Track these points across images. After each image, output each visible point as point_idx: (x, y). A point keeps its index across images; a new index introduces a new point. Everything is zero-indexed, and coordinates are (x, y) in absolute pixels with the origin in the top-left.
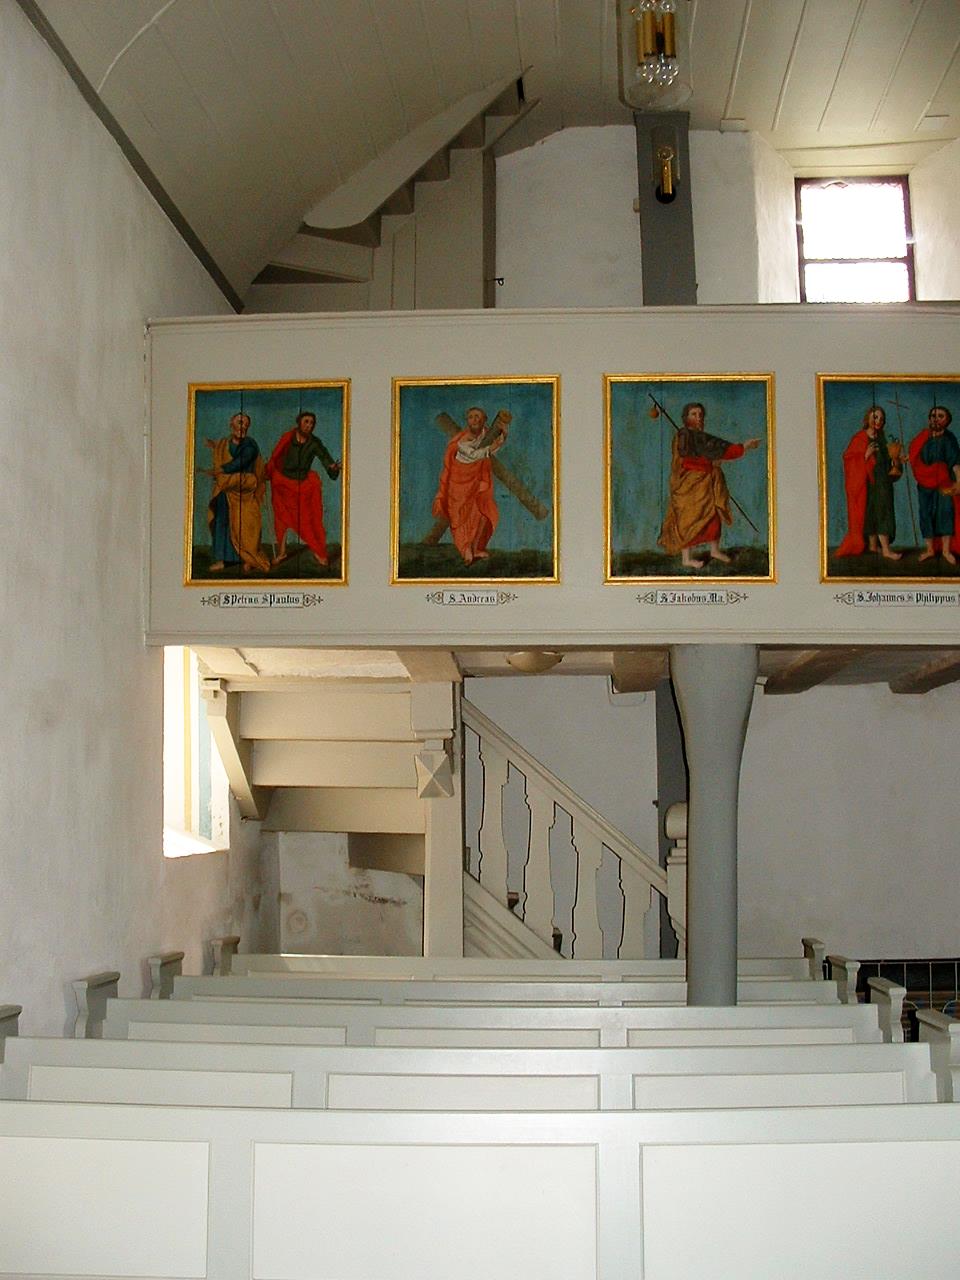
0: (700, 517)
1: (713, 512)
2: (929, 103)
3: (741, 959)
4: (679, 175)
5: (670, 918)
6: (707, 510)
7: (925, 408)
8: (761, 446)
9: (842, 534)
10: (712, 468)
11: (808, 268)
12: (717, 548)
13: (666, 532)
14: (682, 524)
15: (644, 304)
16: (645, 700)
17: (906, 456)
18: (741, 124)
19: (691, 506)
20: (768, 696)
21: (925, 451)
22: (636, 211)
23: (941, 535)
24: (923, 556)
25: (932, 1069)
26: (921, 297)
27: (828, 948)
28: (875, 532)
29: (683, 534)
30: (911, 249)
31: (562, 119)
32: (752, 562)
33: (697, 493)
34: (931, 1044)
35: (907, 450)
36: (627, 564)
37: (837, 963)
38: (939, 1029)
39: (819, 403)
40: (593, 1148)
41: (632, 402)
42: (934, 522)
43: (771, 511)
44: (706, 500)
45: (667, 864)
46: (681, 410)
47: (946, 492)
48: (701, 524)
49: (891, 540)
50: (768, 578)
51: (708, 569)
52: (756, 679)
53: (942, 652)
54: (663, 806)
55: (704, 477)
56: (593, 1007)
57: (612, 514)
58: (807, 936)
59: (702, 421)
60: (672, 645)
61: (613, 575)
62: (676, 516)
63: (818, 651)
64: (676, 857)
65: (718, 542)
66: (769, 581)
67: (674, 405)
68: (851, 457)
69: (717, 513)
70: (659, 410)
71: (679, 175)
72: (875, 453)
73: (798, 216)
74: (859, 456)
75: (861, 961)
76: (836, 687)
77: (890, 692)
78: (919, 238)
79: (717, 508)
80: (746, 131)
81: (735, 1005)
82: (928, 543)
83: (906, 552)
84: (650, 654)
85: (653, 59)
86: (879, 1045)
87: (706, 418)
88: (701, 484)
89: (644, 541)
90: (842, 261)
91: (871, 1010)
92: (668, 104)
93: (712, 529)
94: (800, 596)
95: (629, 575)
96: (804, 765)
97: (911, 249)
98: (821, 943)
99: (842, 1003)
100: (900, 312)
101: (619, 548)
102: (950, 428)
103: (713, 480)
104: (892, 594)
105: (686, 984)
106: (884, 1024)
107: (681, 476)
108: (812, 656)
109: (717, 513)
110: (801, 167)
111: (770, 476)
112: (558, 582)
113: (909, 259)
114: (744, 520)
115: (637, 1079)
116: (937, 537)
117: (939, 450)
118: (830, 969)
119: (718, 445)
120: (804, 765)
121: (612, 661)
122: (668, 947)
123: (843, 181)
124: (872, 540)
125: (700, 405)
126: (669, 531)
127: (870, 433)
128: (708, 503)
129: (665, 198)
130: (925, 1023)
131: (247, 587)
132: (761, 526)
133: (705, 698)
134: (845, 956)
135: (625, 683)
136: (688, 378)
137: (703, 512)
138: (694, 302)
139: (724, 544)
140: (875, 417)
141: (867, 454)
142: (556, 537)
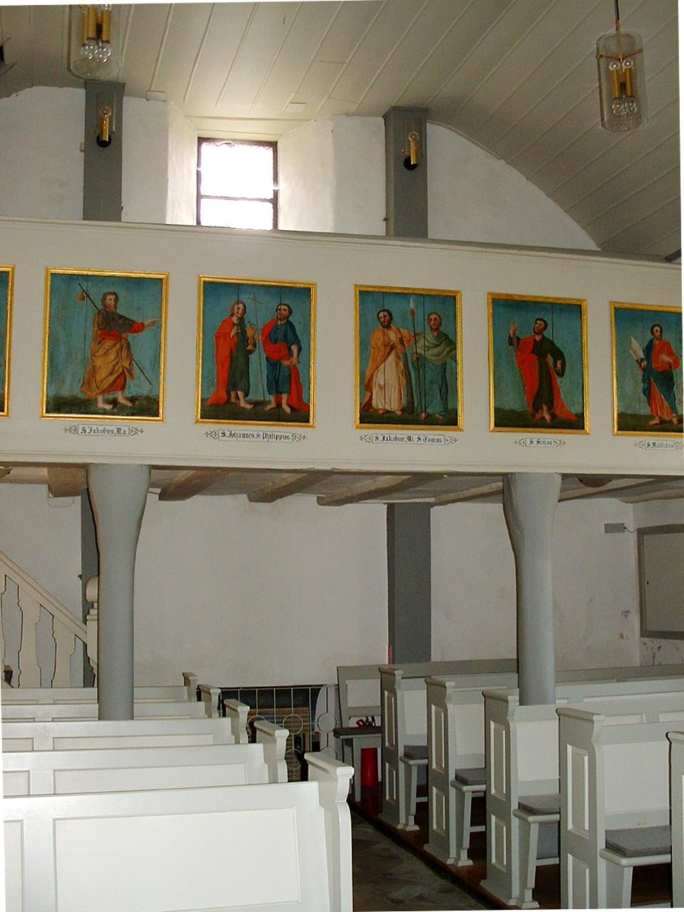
0: (111, 374)
1: (121, 370)
2: (293, 94)
3: (136, 687)
4: (114, 128)
5: (89, 658)
6: (117, 368)
7: (274, 304)
8: (157, 324)
9: (213, 389)
10: (121, 339)
11: (203, 201)
12: (123, 395)
13: (87, 383)
14: (98, 378)
15: (84, 219)
16: (74, 502)
17: (259, 338)
18: (162, 96)
19: (106, 365)
20: (161, 502)
21: (273, 334)
22: (82, 151)
23: (281, 393)
24: (268, 408)
25: (265, 761)
26: (281, 227)
27: (200, 680)
28: (235, 387)
29: (99, 385)
30: (276, 193)
31: (31, 79)
32: (148, 407)
33: (110, 356)
34: (264, 744)
35: (260, 332)
36: (58, 405)
37: (205, 689)
38: (269, 734)
39: (611, 328)
40: (20, 823)
41: (65, 287)
42: (277, 383)
43: (162, 371)
44: (116, 361)
45: (87, 620)
46: (101, 296)
47: (286, 363)
48: (112, 378)
49: (246, 395)
50: (158, 418)
51: (116, 410)
52: (148, 488)
53: (282, 474)
54: (84, 578)
55: (115, 345)
56: (32, 722)
57: (48, 369)
58: (185, 671)
59: (116, 304)
60: (90, 464)
61: (47, 412)
62: (94, 371)
63: (194, 471)
64: (92, 615)
65: (123, 391)
66: (158, 420)
67: (96, 292)
68: (221, 336)
69: (123, 371)
70: (85, 296)
71: (114, 128)
72: (236, 334)
73: (198, 165)
74: (226, 335)
75: (221, 688)
76: (210, 497)
77: (248, 501)
78: (283, 186)
79: (124, 367)
80: (165, 101)
81: (133, 719)
82: (272, 398)
83: (256, 404)
84: (73, 470)
85: (95, 42)
86: (232, 746)
87: (119, 303)
88: (114, 349)
89: (70, 388)
90: (227, 198)
91: (227, 721)
92: (103, 75)
93: (120, 382)
94: (601, 446)
95: (59, 413)
96: (178, 554)
97: (276, 193)
98: (194, 675)
99: (209, 717)
100: (267, 236)
101: (52, 393)
102: (290, 319)
103: (122, 346)
104: (245, 432)
105: (98, 705)
106: (235, 731)
107: (99, 343)
108: (189, 475)
109: (123, 371)
110: (202, 130)
111: (163, 346)
112: (162, 420)
113: (275, 201)
114: (142, 378)
115: (56, 772)
116: (278, 394)
117: (282, 333)
118: (200, 694)
119: (126, 322)
120: (178, 554)
121: (46, 474)
122: (90, 678)
123: (231, 142)
124: (233, 394)
125: (114, 294)
126: (89, 382)
127: (235, 319)
128: (117, 363)
129: (103, 144)
130: (260, 730)
131: (267, 427)
132: (154, 380)
133: (114, 504)
134: (209, 684)
135: (58, 491)
136: (107, 274)
137: (113, 370)
138: (120, 221)
139: (127, 393)
140: (239, 309)
141: (232, 334)
142: (7, 383)
